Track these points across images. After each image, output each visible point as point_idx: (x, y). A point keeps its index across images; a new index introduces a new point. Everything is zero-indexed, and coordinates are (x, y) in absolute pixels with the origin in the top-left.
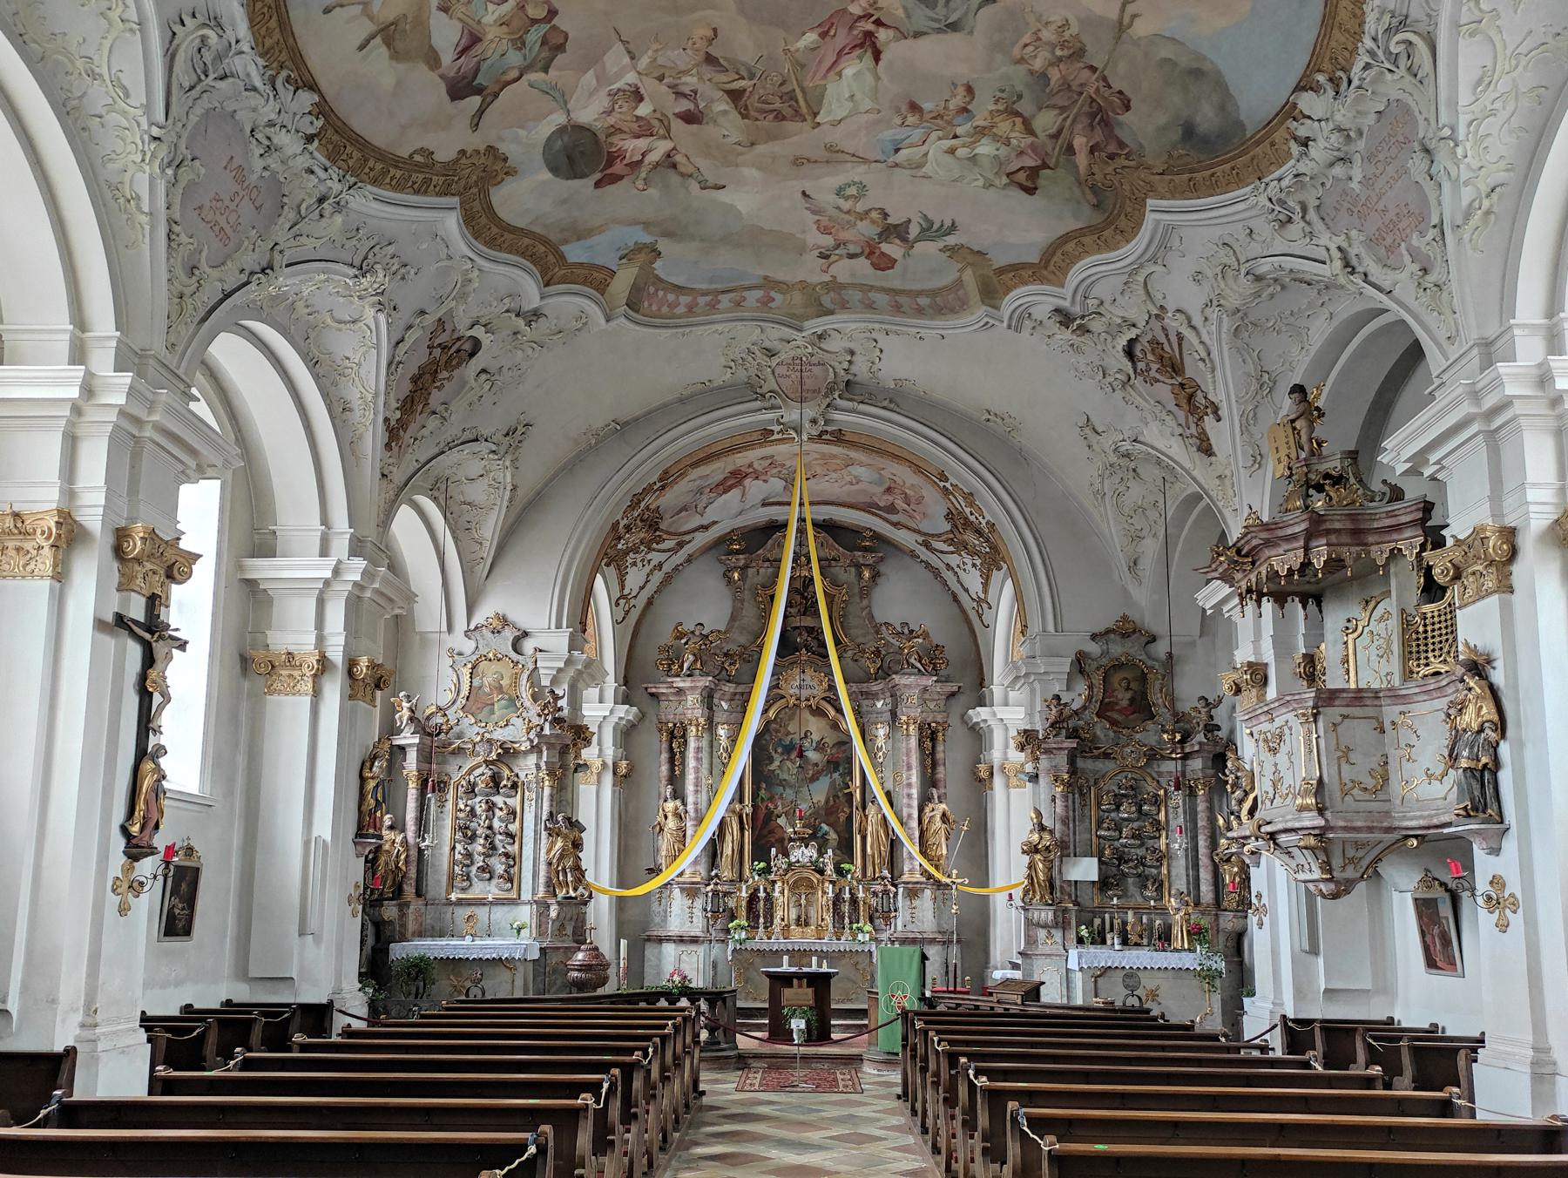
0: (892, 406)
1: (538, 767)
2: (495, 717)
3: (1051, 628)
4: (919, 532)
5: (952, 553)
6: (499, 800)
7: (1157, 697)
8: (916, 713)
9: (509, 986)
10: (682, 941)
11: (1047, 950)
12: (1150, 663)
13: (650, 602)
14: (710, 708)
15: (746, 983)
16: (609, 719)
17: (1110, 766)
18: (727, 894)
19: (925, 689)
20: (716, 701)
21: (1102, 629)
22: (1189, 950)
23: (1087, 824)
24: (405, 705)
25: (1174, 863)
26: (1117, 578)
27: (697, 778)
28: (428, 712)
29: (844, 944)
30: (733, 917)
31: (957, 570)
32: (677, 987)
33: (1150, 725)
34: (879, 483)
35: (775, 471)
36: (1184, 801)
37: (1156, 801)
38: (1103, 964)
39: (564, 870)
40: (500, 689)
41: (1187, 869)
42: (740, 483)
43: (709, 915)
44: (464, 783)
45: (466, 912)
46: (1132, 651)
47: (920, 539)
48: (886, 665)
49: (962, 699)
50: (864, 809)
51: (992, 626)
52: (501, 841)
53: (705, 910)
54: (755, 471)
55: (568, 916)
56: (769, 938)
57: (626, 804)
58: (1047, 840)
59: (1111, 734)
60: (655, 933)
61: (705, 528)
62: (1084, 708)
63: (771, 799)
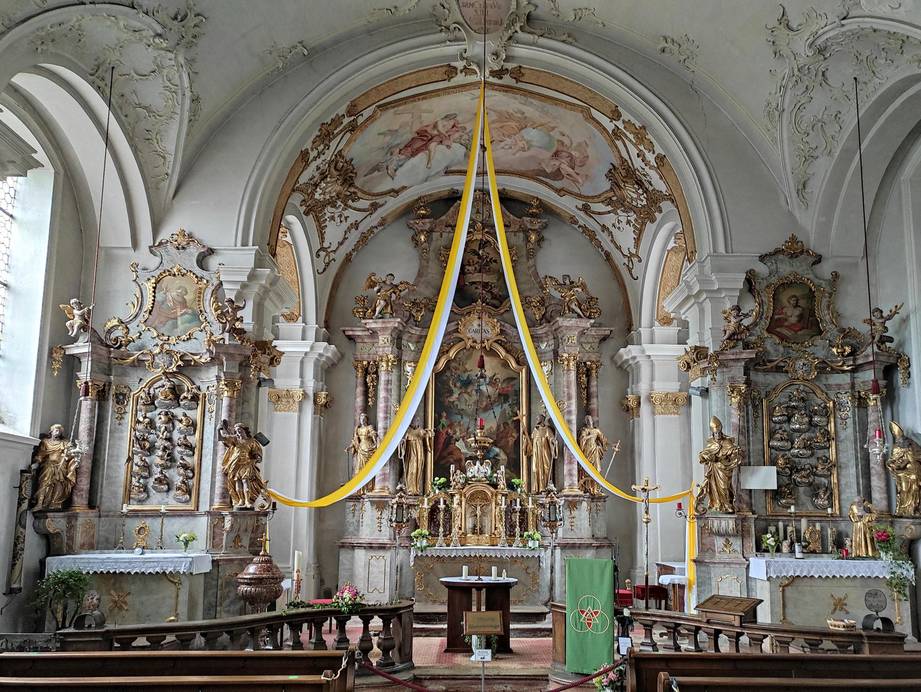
0: (570, 40)
1: (218, 378)
2: (178, 331)
3: (721, 249)
4: (579, 196)
5: (609, 212)
6: (178, 412)
7: (823, 314)
8: (576, 350)
9: (173, 601)
10: (371, 547)
11: (725, 557)
12: (816, 281)
13: (348, 259)
14: (399, 347)
15: (427, 586)
16: (309, 356)
17: (780, 379)
18: (410, 506)
19: (582, 333)
20: (404, 342)
21: (772, 250)
22: (874, 558)
23: (759, 435)
24: (76, 312)
25: (844, 472)
26: (784, 204)
27: (387, 407)
28: (109, 325)
29: (516, 550)
30: (416, 527)
31: (612, 229)
32: (347, 605)
33: (818, 341)
34: (546, 147)
35: (457, 135)
36: (854, 412)
37: (826, 413)
38: (791, 573)
39: (240, 480)
40: (184, 304)
41: (858, 477)
42: (425, 147)
43: (394, 524)
44: (143, 395)
45: (137, 524)
46: (800, 271)
47: (580, 203)
48: (548, 315)
49: (611, 343)
50: (530, 434)
51: (640, 279)
52: (181, 453)
53: (391, 520)
54: (440, 134)
55: (243, 527)
56: (448, 545)
57: (327, 430)
58: (728, 449)
59: (781, 349)
60: (349, 541)
61: (395, 192)
62: (755, 324)
63: (451, 426)
